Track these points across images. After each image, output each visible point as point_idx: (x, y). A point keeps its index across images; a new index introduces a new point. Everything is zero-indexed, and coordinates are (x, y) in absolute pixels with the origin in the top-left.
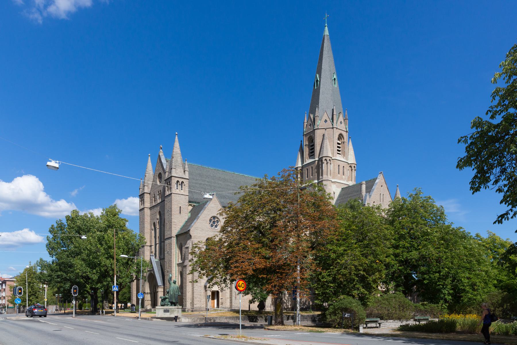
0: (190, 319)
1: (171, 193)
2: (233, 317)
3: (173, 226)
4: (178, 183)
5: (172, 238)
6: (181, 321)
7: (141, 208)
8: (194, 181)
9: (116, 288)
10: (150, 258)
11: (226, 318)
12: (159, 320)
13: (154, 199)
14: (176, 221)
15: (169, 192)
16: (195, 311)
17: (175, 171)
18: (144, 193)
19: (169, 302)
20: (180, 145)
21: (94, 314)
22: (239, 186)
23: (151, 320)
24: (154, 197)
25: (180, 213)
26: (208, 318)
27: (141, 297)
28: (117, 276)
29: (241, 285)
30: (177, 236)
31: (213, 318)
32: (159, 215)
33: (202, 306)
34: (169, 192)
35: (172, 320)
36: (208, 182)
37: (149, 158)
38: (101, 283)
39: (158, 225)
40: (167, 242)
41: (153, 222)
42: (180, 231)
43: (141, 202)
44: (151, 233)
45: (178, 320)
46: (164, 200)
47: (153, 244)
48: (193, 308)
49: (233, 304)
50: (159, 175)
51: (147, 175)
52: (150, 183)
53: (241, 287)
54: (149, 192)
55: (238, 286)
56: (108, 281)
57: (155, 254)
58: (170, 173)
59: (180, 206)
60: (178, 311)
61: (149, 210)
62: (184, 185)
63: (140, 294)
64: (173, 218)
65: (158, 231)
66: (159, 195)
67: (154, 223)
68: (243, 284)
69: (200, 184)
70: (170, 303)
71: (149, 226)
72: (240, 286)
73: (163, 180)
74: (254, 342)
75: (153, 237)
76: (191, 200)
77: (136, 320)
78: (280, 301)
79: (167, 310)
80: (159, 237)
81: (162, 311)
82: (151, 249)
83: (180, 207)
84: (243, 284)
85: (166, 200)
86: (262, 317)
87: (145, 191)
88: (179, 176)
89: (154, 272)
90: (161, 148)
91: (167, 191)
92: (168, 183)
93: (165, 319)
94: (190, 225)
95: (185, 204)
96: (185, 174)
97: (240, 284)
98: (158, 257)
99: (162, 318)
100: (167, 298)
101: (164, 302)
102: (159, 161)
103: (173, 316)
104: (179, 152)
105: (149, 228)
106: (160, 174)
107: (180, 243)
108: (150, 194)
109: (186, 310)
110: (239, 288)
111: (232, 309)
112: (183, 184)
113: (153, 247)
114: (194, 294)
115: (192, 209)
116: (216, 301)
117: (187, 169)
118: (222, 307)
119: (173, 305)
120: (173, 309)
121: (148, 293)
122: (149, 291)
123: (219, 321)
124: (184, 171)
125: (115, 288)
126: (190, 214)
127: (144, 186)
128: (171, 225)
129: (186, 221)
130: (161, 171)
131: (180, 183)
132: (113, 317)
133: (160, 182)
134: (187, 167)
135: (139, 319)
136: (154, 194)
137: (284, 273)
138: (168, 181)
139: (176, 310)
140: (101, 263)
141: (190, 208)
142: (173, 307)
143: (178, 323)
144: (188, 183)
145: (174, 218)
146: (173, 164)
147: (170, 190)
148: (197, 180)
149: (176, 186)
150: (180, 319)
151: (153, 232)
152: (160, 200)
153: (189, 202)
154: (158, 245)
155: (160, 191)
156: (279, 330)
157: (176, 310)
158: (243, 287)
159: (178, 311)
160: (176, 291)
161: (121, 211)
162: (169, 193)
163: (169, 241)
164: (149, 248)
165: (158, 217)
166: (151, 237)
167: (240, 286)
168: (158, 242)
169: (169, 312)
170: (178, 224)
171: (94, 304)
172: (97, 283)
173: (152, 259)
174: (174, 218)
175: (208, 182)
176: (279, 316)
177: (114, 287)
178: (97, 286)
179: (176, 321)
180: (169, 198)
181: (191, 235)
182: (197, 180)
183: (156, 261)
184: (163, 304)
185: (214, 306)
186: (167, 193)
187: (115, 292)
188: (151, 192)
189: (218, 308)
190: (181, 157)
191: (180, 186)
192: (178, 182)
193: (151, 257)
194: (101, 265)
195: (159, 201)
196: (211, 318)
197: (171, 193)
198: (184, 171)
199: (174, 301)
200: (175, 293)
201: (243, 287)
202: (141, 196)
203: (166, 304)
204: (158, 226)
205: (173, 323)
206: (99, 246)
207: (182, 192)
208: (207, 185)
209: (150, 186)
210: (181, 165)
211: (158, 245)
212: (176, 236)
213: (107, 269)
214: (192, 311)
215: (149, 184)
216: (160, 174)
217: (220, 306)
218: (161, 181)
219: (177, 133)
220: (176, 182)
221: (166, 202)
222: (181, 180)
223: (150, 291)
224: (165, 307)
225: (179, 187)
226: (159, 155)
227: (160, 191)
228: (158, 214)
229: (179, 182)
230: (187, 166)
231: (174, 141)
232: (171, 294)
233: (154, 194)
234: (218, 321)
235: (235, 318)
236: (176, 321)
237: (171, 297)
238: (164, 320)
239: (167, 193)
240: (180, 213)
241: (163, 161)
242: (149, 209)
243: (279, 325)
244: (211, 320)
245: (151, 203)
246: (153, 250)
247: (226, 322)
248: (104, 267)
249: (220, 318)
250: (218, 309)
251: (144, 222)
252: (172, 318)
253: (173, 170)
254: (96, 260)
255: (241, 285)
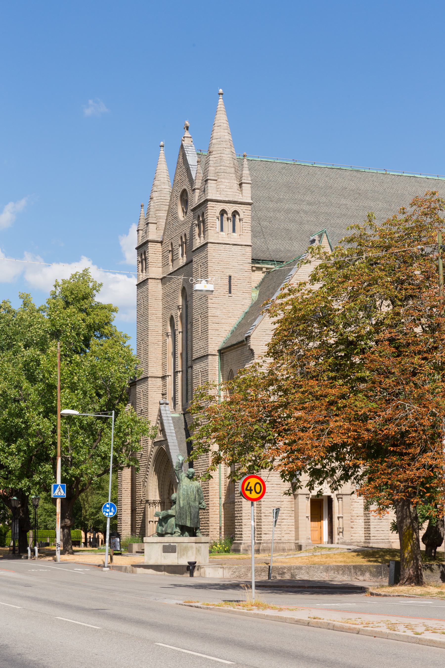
0: (226, 571)
1: (207, 244)
2: (345, 566)
3: (211, 326)
4: (225, 215)
5: (210, 357)
6: (203, 575)
7: (141, 280)
8: (271, 205)
9: (62, 491)
10: (160, 411)
11: (327, 569)
12: (151, 571)
13: (170, 255)
14: (218, 313)
15: (202, 238)
16: (264, 550)
17: (215, 185)
18: (207, 201)
19: (177, 525)
20: (230, 120)
21: (19, 557)
22: (398, 208)
23: (133, 572)
24: (172, 251)
25: (230, 292)
26: (277, 569)
27: (111, 514)
28: (62, 457)
29: (253, 488)
30: (222, 352)
31: (290, 569)
32: (182, 296)
33: (286, 538)
34: (202, 238)
35: (182, 573)
36: (310, 204)
37: (162, 152)
38: (30, 477)
39: (179, 323)
40: (197, 367)
41: (169, 316)
42: (229, 339)
43: (140, 265)
44: (164, 342)
45: (196, 573)
46: (191, 261)
47: (170, 372)
48: (260, 543)
49: (373, 532)
50: (182, 196)
51: (155, 195)
52: (163, 214)
53: (253, 492)
54: (160, 239)
55: (247, 490)
56: (45, 472)
57: (174, 399)
58: (204, 191)
59: (228, 274)
60: (198, 550)
61: (160, 285)
62: (240, 220)
63: (108, 506)
64: (210, 305)
65: (179, 337)
66: (182, 246)
67: (172, 318)
68: (258, 486)
69: (289, 211)
70: (178, 530)
71: (161, 324)
72: (251, 490)
73: (190, 208)
74: (267, 616)
75: (170, 354)
76: (261, 256)
77: (97, 572)
78: (412, 523)
79: (170, 546)
80: (181, 354)
81: (159, 548)
82: (165, 385)
83: (230, 277)
84: (258, 486)
85: (194, 259)
86: (432, 570)
87: (150, 238)
88: (227, 199)
89: (167, 446)
90: (187, 128)
91: (197, 237)
92: (199, 217)
93: (165, 571)
94: (251, 324)
95: (241, 267)
96: (241, 191)
97: (252, 485)
98: (181, 407)
99: (157, 568)
100: (172, 516)
101: (165, 526)
102: (181, 160)
103: (184, 562)
104: (228, 137)
105: (161, 332)
106: (184, 193)
107: (229, 370)
108: (161, 242)
109: (242, 547)
110: (247, 493)
111: (371, 545)
112: (237, 216)
113: (170, 380)
114: (262, 506)
115: (263, 279)
116: (325, 523)
117: (247, 178)
118: (341, 541)
119: (187, 533)
120: (184, 545)
121: (154, 503)
122: (158, 498)
123: (306, 577)
124: (241, 185)
125: (57, 490)
126: (258, 292)
127: (147, 224)
128: (206, 324)
129: (246, 311)
130: (187, 186)
131: (230, 215)
132: (53, 566)
133: (185, 213)
134: (248, 172)
135: (105, 569)
136: (172, 244)
137: (406, 454)
138: (199, 212)
139: (192, 547)
140: (28, 427)
141: (259, 276)
142: (187, 539)
143: (197, 579)
144: (249, 213)
145: (214, 306)
146: (210, 168)
147: (204, 234)
148: (280, 200)
149: (218, 223)
150: (202, 570)
151: (169, 341)
152: (185, 258)
153: (255, 261)
154: (180, 375)
155: (185, 235)
156: (390, 596)
157: (192, 547)
158: (258, 490)
159: (198, 550)
160: (193, 497)
161: (101, 285)
162: (203, 242)
163: (203, 364)
164: (159, 382)
165: (180, 301)
166: (164, 353)
167: (251, 490)
168: (179, 368)
169: (175, 552)
170: (223, 321)
171: (18, 530)
172: (20, 478)
173: (162, 412)
174: (214, 306)
175: (310, 204)
176: (410, 562)
177: (56, 487)
178: (20, 486)
179: (192, 575)
180: (203, 254)
181: (252, 350)
182: (280, 200)
183: (173, 418)
184: (162, 531)
185: (321, 538)
186: (198, 242)
187: (58, 501)
188: (165, 237)
189: (332, 543)
190: (233, 150)
191: (230, 224)
192: (223, 212)
193: (162, 407)
194: (29, 431)
195: (182, 261)
196: (284, 568)
197: (207, 244)
198: (241, 185)
199: (188, 524)
200: (192, 503)
201: (258, 490)
202: (142, 250)
203: (169, 531)
204: (179, 327)
205: (185, 579)
206: (25, 384)
207: (235, 238)
208: (306, 212)
209: (162, 223)
210: (233, 170)
211: (180, 375)
212: (219, 351)
213: (43, 442)
214: (258, 551)
215: (160, 218)
216: (184, 193)
217: (336, 537)
218: (187, 208)
219: (221, 91)
220: (218, 215)
221: (195, 266)
222: (230, 208)
223: (161, 495)
224: (167, 539)
225: (228, 225)
226: (182, 145)
227: (185, 235)
228: (180, 295)
229: (227, 214)
230: (246, 172)
231: (215, 112)
232: (182, 505)
233: (172, 244)
234: (302, 576)
235: (353, 571)
236: (192, 575)
237: (181, 515)
238: (163, 573)
239: (198, 242)
240: (230, 292)
241: (192, 159)
242: (159, 281)
243: (410, 584)
244: (284, 573)
245: (165, 265)
246: (170, 387)
247: (327, 579)
248: (36, 436)
249: (309, 568)
250: (330, 546)
251: (147, 315)
252: (183, 566)
253: (211, 184)
254: (16, 420)
255: (253, 488)
